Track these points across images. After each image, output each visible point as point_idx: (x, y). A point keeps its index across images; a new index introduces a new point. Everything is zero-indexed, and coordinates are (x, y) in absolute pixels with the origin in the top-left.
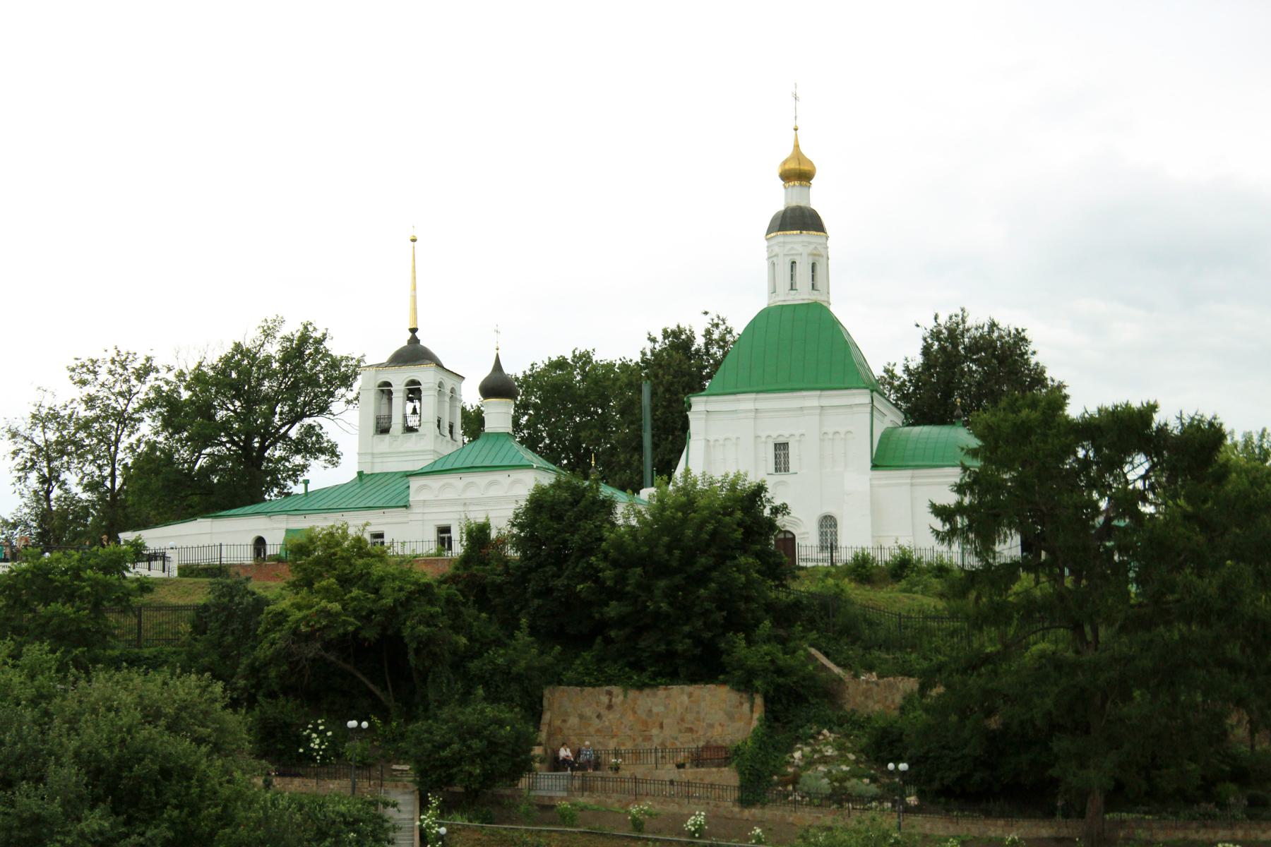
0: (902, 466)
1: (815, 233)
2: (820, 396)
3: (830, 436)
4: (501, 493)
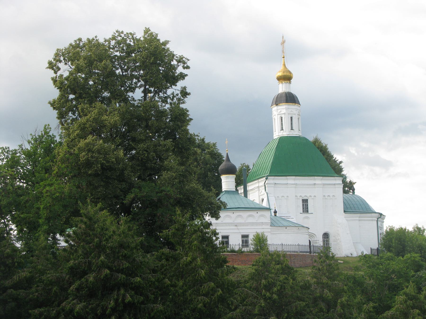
1: (291, 104)
2: (322, 179)
3: (313, 198)
4: (231, 221)
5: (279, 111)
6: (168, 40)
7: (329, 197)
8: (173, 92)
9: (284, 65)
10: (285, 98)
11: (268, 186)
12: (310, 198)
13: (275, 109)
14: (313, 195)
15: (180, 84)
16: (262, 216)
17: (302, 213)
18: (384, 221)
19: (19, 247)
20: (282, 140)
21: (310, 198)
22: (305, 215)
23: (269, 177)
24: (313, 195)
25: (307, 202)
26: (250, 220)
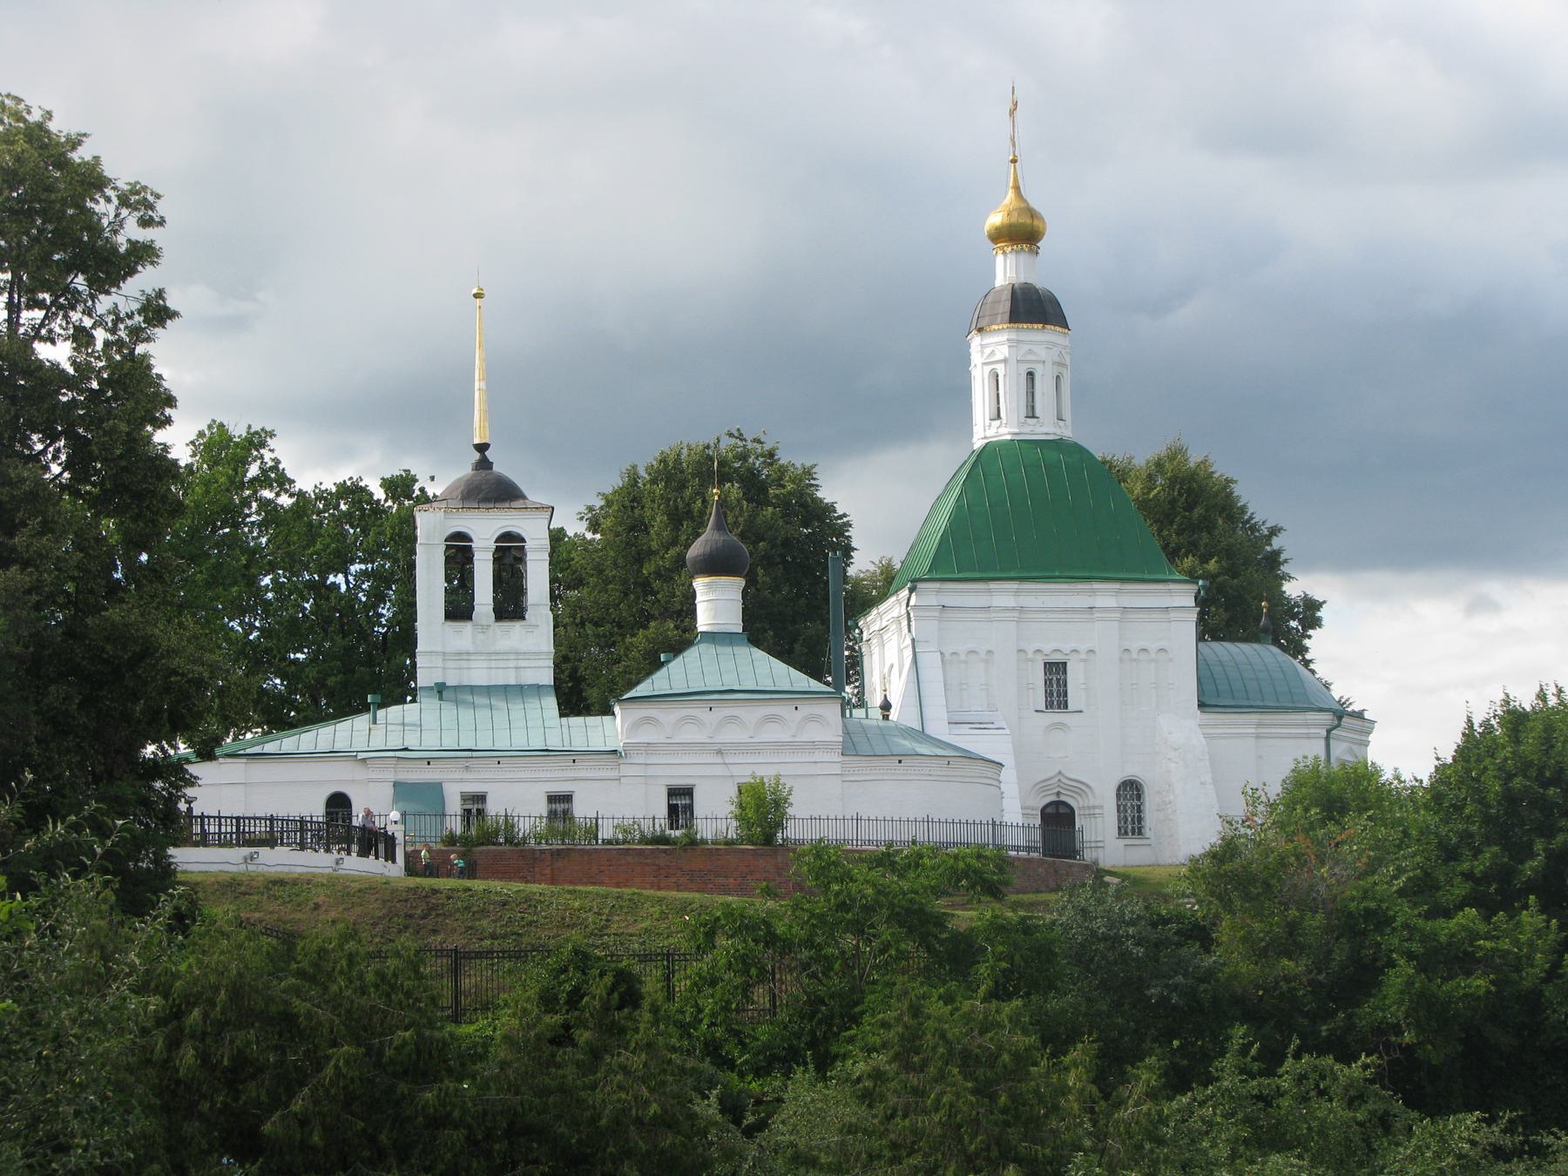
0: (1277, 708)
2: (1017, 591)
3: (1083, 656)
4: (700, 737)
5: (988, 351)
6: (83, 132)
7: (1143, 656)
8: (116, 304)
9: (1017, 188)
10: (1005, 306)
11: (918, 614)
12: (1073, 657)
14: (1153, 647)
17: (1042, 711)
18: (1370, 739)
21: (1073, 657)
22: (1055, 717)
23: (920, 585)
24: (1083, 647)
25: (1065, 672)
26: (773, 734)
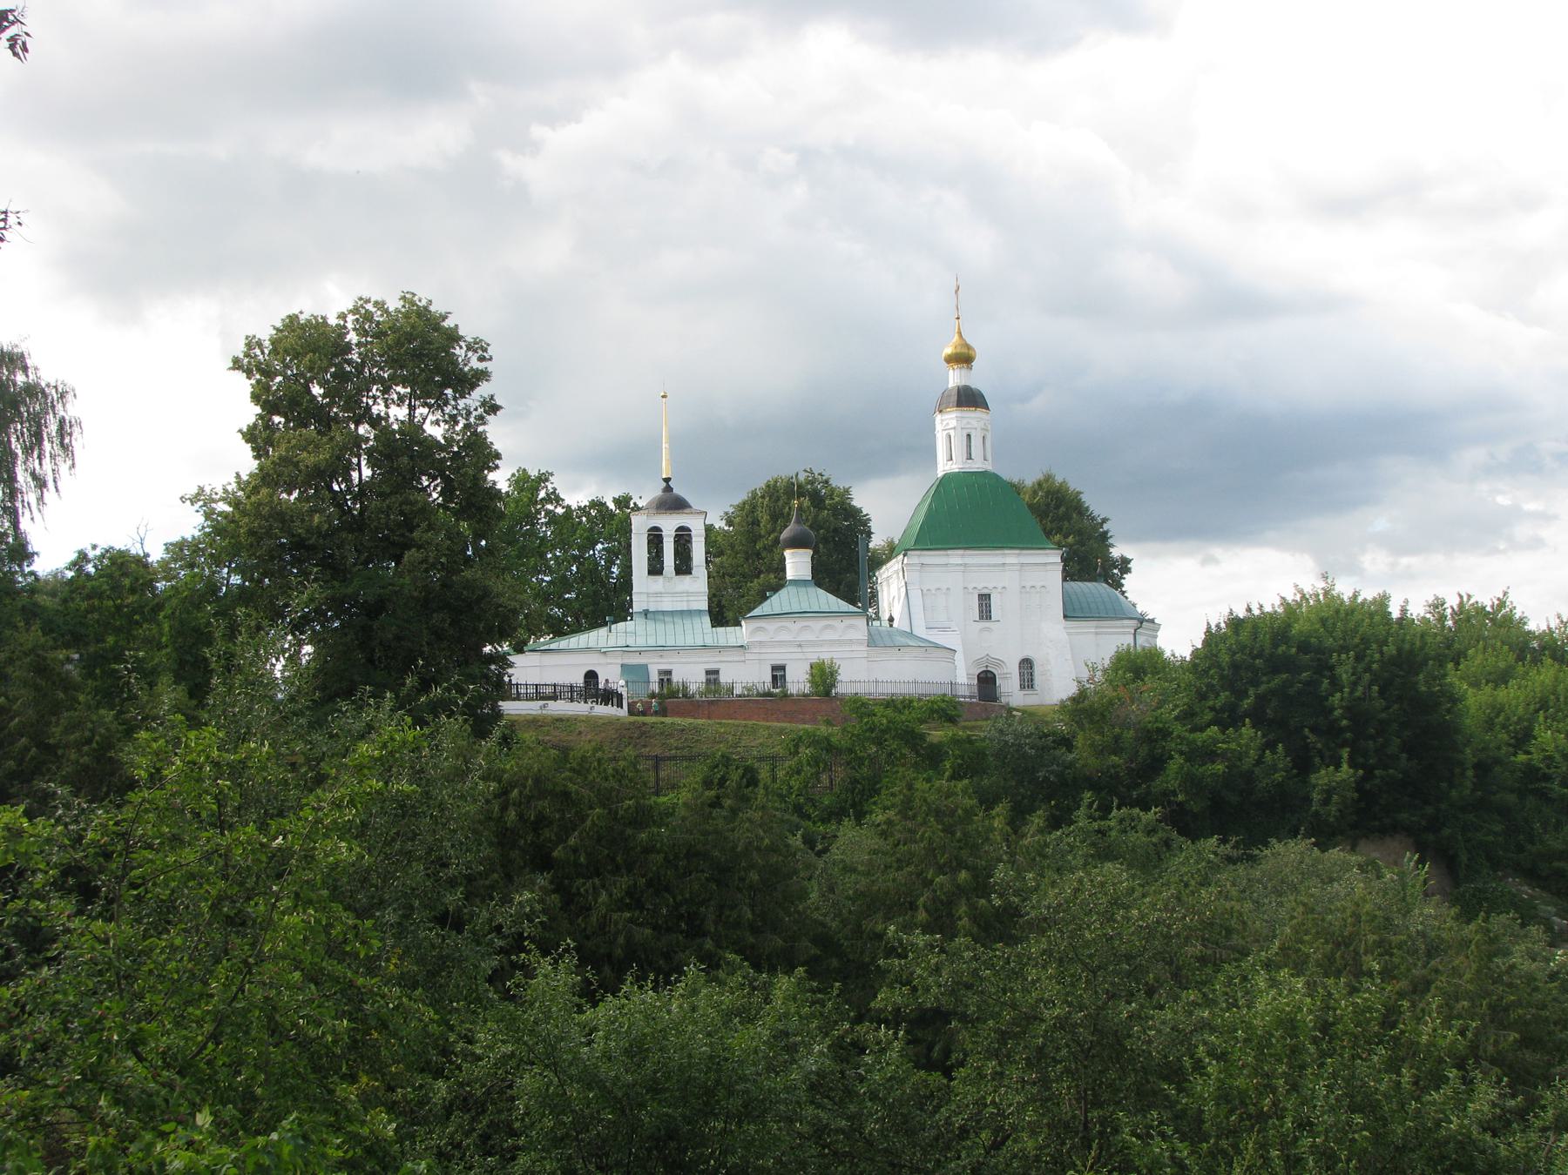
2: (1019, 555)
3: (999, 590)
4: (835, 637)
5: (945, 423)
7: (1033, 590)
9: (960, 333)
13: (938, 417)
14: (1039, 585)
15: (483, 390)
16: (851, 626)
19: (1018, 710)
20: (947, 479)
22: (986, 624)
23: (909, 552)
24: (1000, 586)
